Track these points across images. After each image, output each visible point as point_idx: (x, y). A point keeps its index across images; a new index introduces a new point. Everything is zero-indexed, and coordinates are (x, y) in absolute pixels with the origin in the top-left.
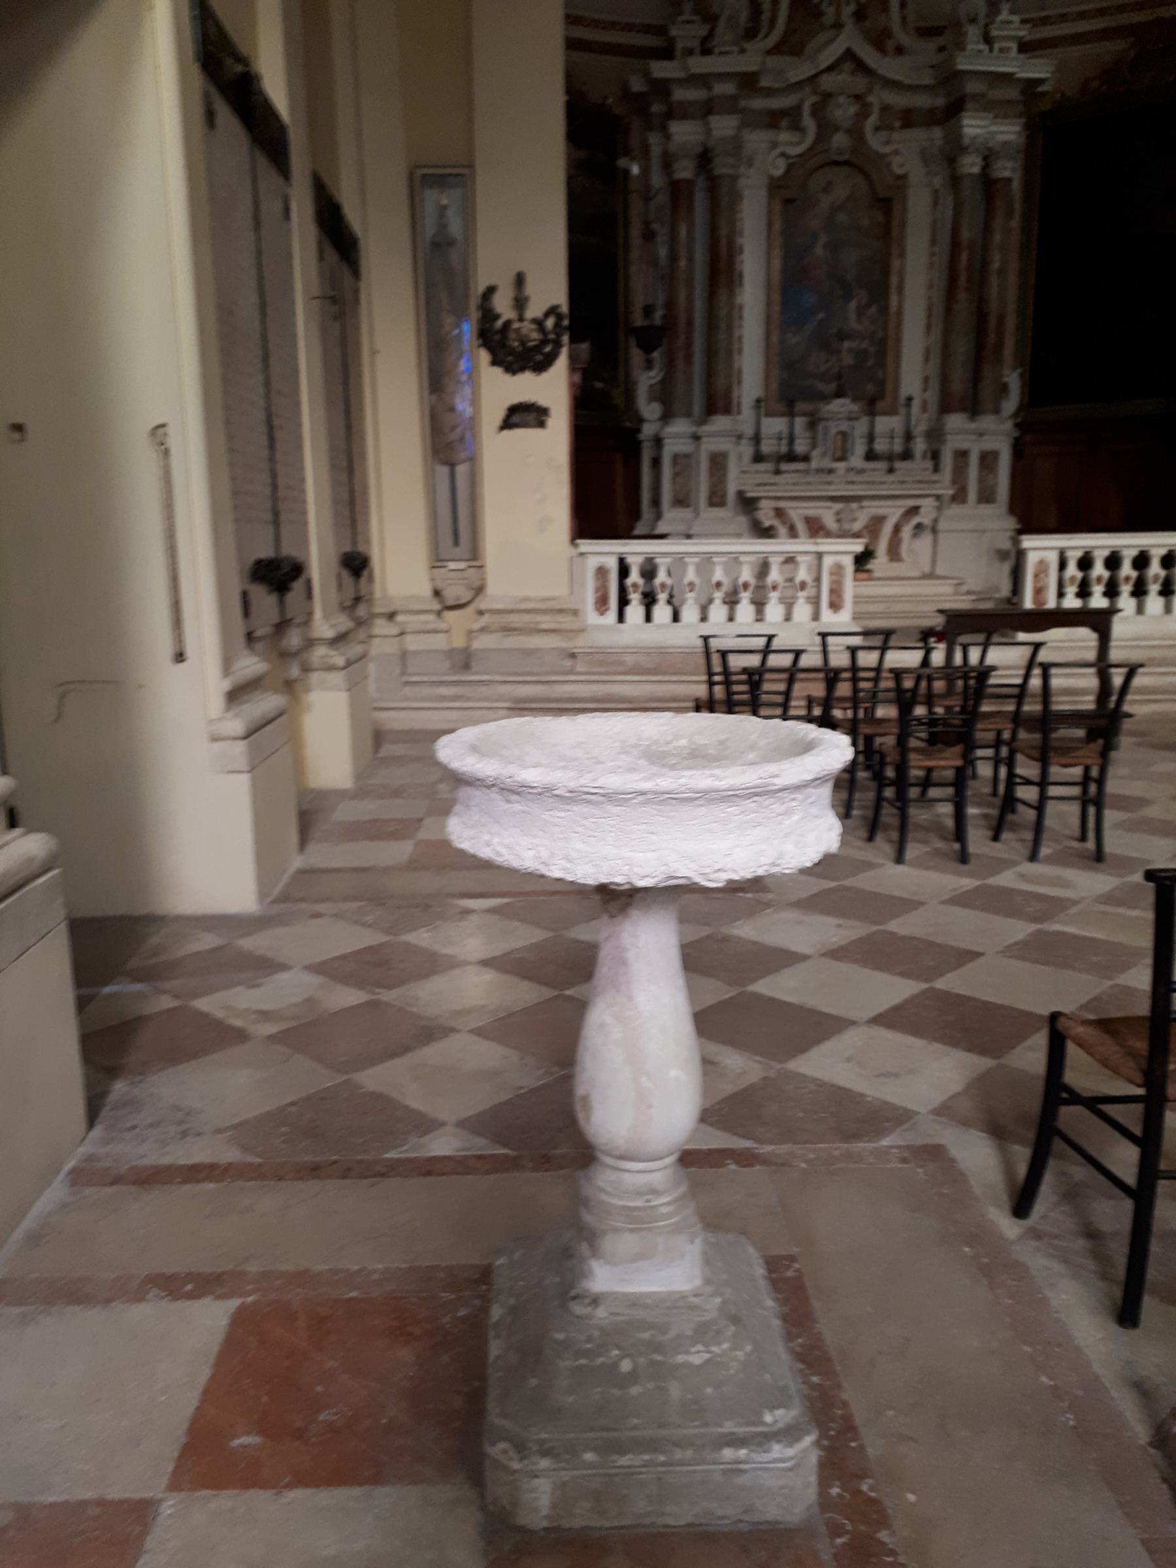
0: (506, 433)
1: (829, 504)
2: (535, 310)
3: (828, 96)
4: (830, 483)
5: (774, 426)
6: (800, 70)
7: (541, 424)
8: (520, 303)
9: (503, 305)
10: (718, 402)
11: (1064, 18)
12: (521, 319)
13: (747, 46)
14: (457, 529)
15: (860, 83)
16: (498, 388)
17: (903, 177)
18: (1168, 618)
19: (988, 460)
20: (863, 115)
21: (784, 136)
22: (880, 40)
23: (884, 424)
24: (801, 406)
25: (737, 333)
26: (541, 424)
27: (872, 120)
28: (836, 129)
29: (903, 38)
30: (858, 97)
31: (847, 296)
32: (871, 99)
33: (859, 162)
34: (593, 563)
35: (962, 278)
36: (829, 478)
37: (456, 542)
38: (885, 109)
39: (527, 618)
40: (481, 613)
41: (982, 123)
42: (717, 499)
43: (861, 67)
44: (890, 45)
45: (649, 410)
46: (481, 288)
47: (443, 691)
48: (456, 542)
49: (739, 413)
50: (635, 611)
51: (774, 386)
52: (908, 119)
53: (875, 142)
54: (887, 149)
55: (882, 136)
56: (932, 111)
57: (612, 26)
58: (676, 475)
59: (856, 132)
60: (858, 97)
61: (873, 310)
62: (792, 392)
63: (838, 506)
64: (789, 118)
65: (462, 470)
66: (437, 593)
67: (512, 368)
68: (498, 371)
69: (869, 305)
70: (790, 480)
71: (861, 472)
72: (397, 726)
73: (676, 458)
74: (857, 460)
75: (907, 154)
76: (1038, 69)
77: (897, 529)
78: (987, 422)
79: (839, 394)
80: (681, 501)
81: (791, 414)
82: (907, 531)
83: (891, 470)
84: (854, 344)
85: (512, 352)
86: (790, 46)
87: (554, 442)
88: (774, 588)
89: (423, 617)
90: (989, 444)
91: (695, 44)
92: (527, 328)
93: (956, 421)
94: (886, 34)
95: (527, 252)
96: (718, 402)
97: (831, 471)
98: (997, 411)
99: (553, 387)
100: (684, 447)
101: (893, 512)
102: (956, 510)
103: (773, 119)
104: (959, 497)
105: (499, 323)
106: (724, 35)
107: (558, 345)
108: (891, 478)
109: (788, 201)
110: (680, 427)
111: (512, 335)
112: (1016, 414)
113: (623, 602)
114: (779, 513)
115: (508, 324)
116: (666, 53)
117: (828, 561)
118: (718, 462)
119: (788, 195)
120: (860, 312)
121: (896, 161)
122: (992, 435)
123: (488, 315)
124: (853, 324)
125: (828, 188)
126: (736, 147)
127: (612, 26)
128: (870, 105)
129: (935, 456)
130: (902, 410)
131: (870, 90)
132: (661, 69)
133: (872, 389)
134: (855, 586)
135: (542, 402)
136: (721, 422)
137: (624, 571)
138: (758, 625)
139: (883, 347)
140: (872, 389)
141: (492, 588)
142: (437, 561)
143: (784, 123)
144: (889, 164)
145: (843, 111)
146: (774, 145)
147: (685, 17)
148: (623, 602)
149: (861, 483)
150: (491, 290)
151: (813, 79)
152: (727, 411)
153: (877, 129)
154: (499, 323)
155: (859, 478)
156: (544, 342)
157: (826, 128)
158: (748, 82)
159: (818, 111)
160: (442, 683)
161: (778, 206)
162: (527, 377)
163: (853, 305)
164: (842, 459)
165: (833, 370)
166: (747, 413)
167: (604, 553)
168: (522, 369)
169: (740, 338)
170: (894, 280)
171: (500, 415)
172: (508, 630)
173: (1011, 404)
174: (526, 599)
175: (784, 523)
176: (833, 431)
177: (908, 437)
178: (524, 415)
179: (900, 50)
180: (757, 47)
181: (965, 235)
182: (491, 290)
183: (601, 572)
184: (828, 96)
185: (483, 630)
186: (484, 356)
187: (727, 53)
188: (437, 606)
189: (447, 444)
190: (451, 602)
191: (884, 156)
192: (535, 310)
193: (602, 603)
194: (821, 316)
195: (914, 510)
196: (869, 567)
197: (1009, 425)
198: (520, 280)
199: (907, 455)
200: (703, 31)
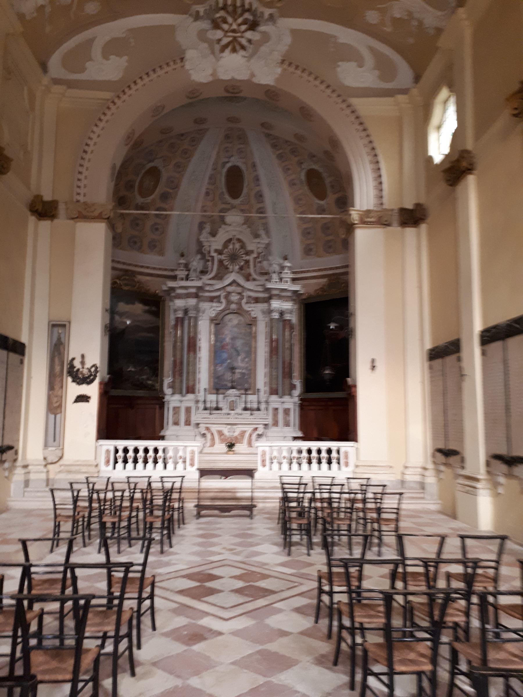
0: (75, 404)
1: (225, 426)
2: (88, 365)
3: (229, 293)
4: (229, 418)
5: (212, 397)
6: (219, 285)
7: (88, 401)
8: (83, 363)
9: (77, 364)
10: (191, 390)
11: (308, 271)
12: (83, 368)
13: (202, 277)
14: (54, 435)
15: (239, 290)
16: (73, 389)
17: (255, 318)
18: (114, 471)
19: (287, 412)
20: (242, 298)
21: (215, 304)
22: (248, 277)
23: (250, 398)
24: (221, 391)
25: (198, 366)
26: (88, 401)
27: (244, 301)
28: (233, 303)
29: (255, 276)
30: (239, 294)
31: (238, 355)
32: (244, 294)
33: (239, 312)
34: (104, 448)
35: (274, 350)
36: (228, 416)
37: (54, 440)
38: (249, 297)
39: (77, 468)
40: (61, 466)
41: (279, 303)
42: (188, 423)
43: (239, 285)
44: (251, 278)
45: (167, 391)
46: (70, 358)
47: (39, 494)
48: (54, 440)
49: (199, 393)
50: (120, 465)
51: (212, 384)
52: (257, 300)
53: (246, 307)
54: (250, 309)
55: (249, 305)
56: (264, 298)
57: (160, 269)
58: (174, 414)
59: (239, 304)
60: (239, 294)
61: (247, 360)
62: (218, 386)
63: (229, 426)
64: (217, 299)
65: (58, 416)
66: (45, 459)
67: (79, 384)
68: (74, 384)
69: (245, 358)
70: (216, 417)
71: (241, 414)
72: (17, 507)
73: (175, 408)
74: (239, 410)
75: (256, 310)
76: (296, 287)
77: (250, 436)
78: (286, 398)
79: (233, 387)
80: (176, 423)
81: (217, 394)
82: (254, 436)
83: (251, 414)
84: (240, 371)
85: (79, 378)
86: (219, 277)
87: (92, 407)
88: (171, 458)
89: (39, 467)
90: (286, 406)
91: (184, 276)
92: (85, 371)
93: (274, 398)
94: (250, 275)
95: (89, 347)
96: (191, 390)
97: (229, 414)
98: (290, 394)
99: (93, 390)
100: (177, 404)
101: (249, 429)
102: (275, 429)
103: (211, 299)
104: (276, 424)
105: (75, 370)
106: (193, 275)
107: (95, 376)
108: (252, 417)
109: (217, 324)
110: (177, 397)
111: (79, 373)
112: (299, 396)
113: (116, 462)
114: (208, 429)
115: (78, 370)
116: (174, 278)
117: (189, 449)
118: (188, 410)
119: (217, 322)
120: (243, 361)
121: (253, 313)
122: (291, 402)
123: (71, 366)
124: (240, 364)
125: (230, 320)
126: (197, 309)
127: (160, 269)
128: (243, 296)
129: (267, 409)
130: (257, 393)
131: (243, 292)
132: (171, 284)
133: (246, 385)
134: (200, 456)
135: (89, 394)
136: (190, 396)
137: (117, 451)
138: (165, 471)
139: (252, 372)
140: (246, 385)
141: (66, 457)
142: (46, 445)
143: (215, 300)
144: (250, 314)
145: (234, 298)
146: (212, 307)
147: (182, 269)
148: (116, 462)
149: (241, 418)
150: (73, 359)
151: (224, 288)
152: (193, 392)
153: (247, 303)
154: (75, 370)
155: (240, 417)
156: (91, 375)
157: (229, 302)
158: (200, 288)
159: (227, 297)
160: (38, 492)
161: (213, 326)
162: (84, 386)
163: (240, 358)
164: (233, 410)
165: (230, 380)
166: (202, 393)
167: (110, 444)
168: (82, 384)
169: (199, 368)
170: (253, 349)
171: (74, 398)
172: (69, 472)
173: (297, 392)
174: (78, 461)
175: (209, 432)
176: (229, 400)
177: (259, 402)
178: (83, 399)
179: (254, 280)
180: (206, 279)
181: (274, 337)
182: (73, 359)
183: (108, 451)
184: (229, 293)
185: (60, 472)
186: (70, 379)
187: (192, 280)
188: (44, 463)
189: (55, 407)
190: (50, 462)
191: (248, 311)
192: (88, 365)
193: (108, 462)
194: (229, 361)
195: (256, 429)
196: (233, 449)
197: (296, 399)
198: (83, 356)
199: (258, 409)
200: (186, 273)
